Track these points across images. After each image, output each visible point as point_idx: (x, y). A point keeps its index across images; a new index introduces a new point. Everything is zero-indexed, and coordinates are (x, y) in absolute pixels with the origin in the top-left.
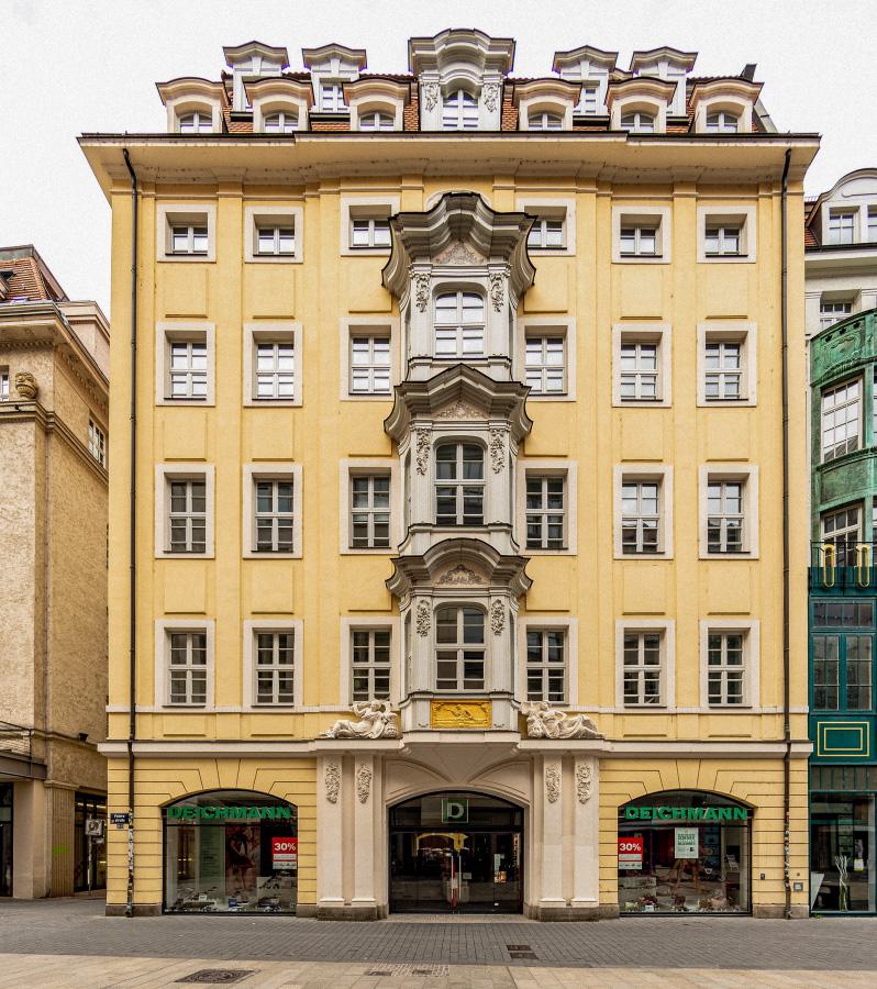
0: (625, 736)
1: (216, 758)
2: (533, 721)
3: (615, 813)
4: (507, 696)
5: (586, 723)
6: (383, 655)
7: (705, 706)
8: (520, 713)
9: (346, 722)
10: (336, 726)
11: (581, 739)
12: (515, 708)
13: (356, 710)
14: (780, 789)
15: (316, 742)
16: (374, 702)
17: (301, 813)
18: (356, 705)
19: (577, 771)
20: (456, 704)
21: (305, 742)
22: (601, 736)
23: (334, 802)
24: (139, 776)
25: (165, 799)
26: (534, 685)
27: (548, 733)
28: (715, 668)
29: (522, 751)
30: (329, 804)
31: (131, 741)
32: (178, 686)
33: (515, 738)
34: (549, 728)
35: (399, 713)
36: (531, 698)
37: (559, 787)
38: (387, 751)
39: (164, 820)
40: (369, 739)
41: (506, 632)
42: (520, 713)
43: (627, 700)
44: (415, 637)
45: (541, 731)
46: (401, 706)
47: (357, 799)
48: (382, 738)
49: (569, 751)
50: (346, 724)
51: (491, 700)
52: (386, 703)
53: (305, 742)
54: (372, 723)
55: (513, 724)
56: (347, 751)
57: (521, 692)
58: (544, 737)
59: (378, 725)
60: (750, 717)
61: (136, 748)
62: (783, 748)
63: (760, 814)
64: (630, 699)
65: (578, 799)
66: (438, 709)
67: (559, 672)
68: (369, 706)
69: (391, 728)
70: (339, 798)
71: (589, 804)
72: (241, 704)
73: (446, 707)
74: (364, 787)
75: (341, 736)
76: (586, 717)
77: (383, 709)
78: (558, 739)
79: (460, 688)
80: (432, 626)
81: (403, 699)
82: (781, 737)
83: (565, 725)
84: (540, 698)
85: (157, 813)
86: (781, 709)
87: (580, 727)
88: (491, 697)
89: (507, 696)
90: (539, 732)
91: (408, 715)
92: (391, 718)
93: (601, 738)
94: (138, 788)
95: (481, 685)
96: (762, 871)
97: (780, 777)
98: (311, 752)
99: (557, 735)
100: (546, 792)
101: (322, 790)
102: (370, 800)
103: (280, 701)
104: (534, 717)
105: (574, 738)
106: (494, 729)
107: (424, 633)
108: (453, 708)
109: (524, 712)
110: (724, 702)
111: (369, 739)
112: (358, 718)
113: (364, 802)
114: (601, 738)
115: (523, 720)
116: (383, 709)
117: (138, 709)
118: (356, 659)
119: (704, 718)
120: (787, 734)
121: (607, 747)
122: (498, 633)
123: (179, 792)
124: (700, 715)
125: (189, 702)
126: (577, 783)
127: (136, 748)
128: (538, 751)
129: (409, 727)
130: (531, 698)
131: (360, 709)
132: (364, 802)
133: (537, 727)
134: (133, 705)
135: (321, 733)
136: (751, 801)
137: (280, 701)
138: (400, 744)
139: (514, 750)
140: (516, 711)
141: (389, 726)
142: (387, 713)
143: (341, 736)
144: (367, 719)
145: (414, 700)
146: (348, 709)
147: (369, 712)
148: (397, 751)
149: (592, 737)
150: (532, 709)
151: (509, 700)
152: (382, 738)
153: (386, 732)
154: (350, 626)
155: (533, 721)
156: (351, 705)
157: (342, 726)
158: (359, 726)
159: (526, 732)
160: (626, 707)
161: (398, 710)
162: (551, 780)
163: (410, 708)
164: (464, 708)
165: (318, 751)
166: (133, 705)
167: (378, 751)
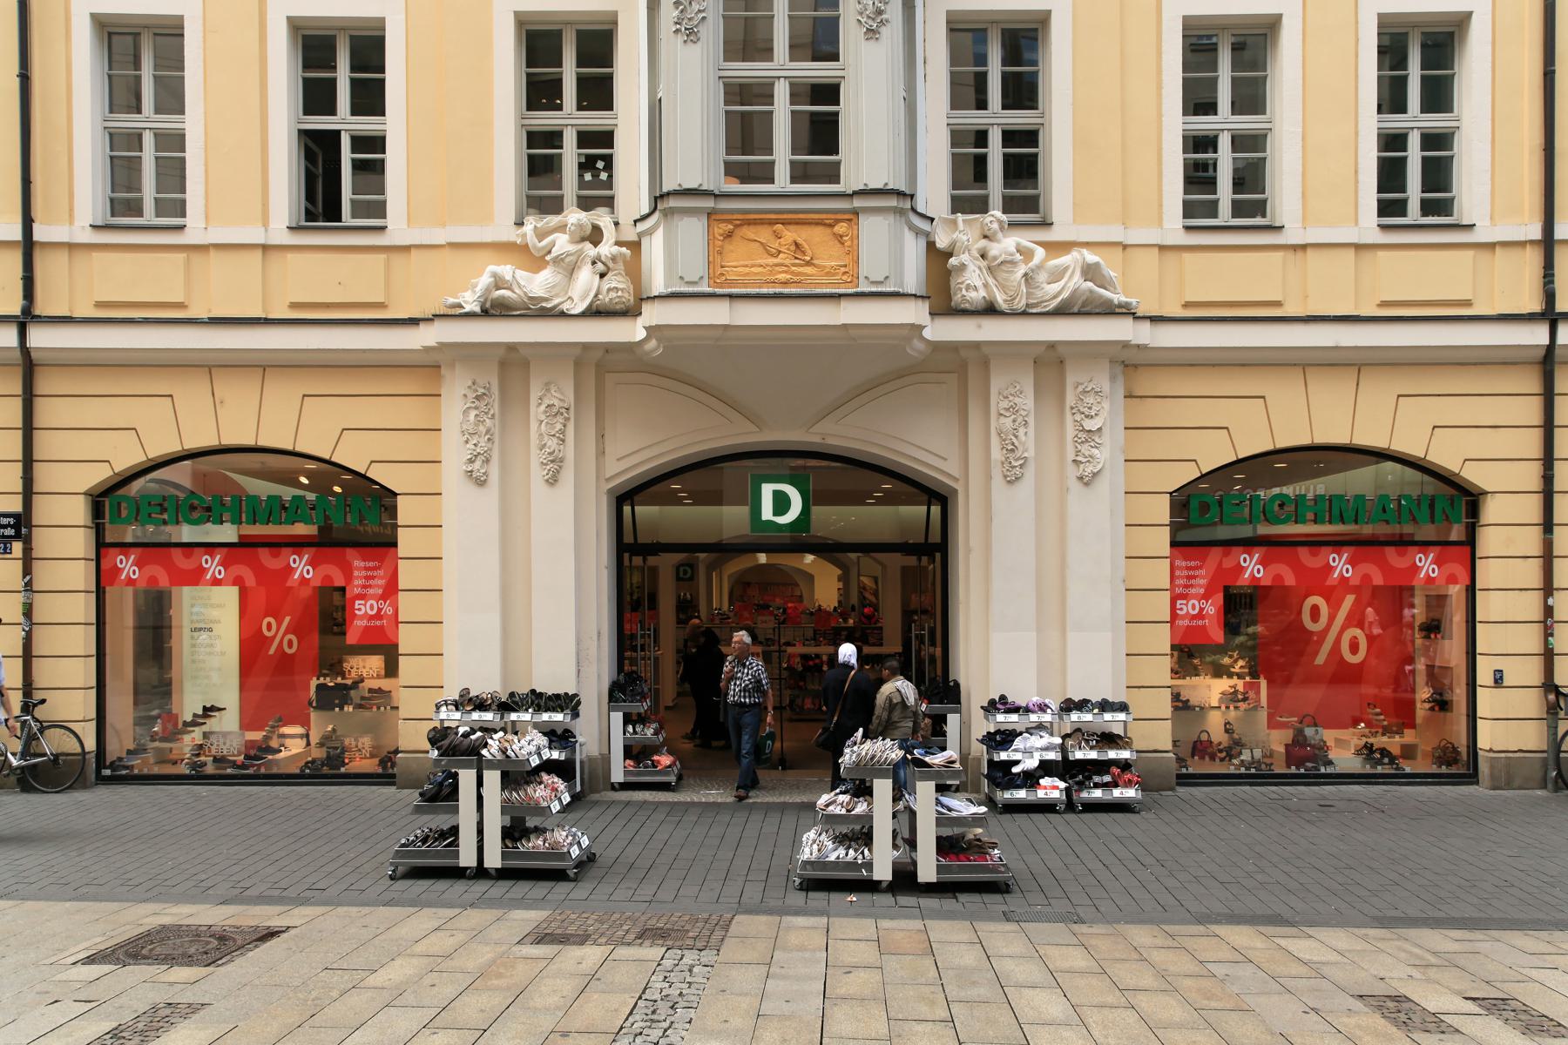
0: (1187, 305)
1: (210, 366)
2: (963, 267)
3: (1161, 510)
4: (900, 199)
5: (1090, 272)
6: (598, 93)
7: (1368, 224)
8: (931, 246)
9: (506, 271)
10: (485, 280)
11: (1080, 314)
12: (918, 232)
13: (531, 239)
14: (1531, 443)
15: (438, 324)
16: (574, 216)
17: (406, 510)
18: (532, 223)
19: (1070, 399)
20: (772, 223)
21: (413, 322)
22: (1127, 305)
23: (481, 482)
24: (46, 413)
25: (98, 476)
26: (971, 170)
27: (1000, 299)
28: (1203, 123)
29: (938, 347)
30: (471, 488)
31: (25, 320)
32: (123, 172)
33: (912, 313)
34: (1003, 287)
35: (635, 246)
36: (959, 205)
37: (1027, 441)
38: (609, 348)
39: (99, 530)
40: (563, 315)
41: (893, 32)
42: (931, 246)
43: (1189, 210)
44: (671, 43)
45: (982, 293)
46: (641, 227)
47: (538, 474)
48: (596, 312)
49: (1052, 346)
50: (508, 277)
51: (856, 212)
52: (602, 218)
53: (413, 322)
54: (571, 271)
55: (913, 274)
56: (512, 347)
57: (935, 190)
58: (990, 310)
59: (586, 278)
60: (1279, 255)
61: (40, 338)
62: (1537, 335)
63: (1492, 511)
64: (1197, 209)
65: (1072, 472)
66: (729, 236)
67: (1030, 137)
68: (562, 228)
69: (617, 287)
70: (494, 471)
71: (1102, 486)
72: (266, 224)
73: (749, 232)
74: (552, 444)
75: (493, 310)
76: (1091, 257)
77: (595, 236)
78: (1024, 314)
79: (782, 180)
80: (710, 15)
81: (646, 210)
82: (1535, 305)
83: (1042, 277)
84: (981, 206)
85: (79, 511)
86: (1535, 232)
87: (1074, 283)
88: (858, 203)
89: (900, 199)
90: (976, 296)
91: (655, 250)
92: (614, 259)
93: (1125, 311)
94: (45, 445)
95: (832, 174)
96: (1499, 663)
97: (1532, 411)
98: (427, 350)
99: (1020, 304)
100: (997, 454)
101: (454, 451)
102: (568, 476)
103: (794, 180)
104: (965, 258)
105: (1062, 311)
106: (864, 288)
107: (691, 35)
108: (764, 234)
109: (942, 242)
110: (1414, 212)
111: (563, 315)
112: (535, 260)
113: (553, 481)
114: (1125, 311)
115: (938, 258)
116: (595, 236)
117: (39, 234)
118: (533, 104)
119: (1171, 257)
120: (1550, 297)
121: (1143, 334)
122: (872, 33)
123: (127, 457)
124: (1162, 248)
125: (149, 216)
126: (1070, 431)
127: (40, 338)
128: (977, 345)
129: (658, 285)
130: (959, 205)
131: (541, 234)
132: (553, 481)
133: (973, 284)
134: (28, 222)
135: (451, 300)
136: (1474, 475)
137: (794, 180)
138: (632, 331)
139: (917, 344)
140: (922, 243)
141: (613, 281)
142: (606, 249)
143: (493, 310)
144: (558, 261)
145: (669, 213)
146: (509, 234)
147: (562, 244)
148: (629, 348)
149: (1110, 311)
150: (961, 234)
151: (900, 212)
152: (596, 312)
153: (605, 298)
154: (516, 14)
155: (963, 267)
156: (520, 224)
157: (499, 283)
158: (537, 284)
159: (948, 296)
160: (1188, 228)
161: (633, 237)
162: (1007, 423)
163: (658, 237)
164: (790, 234)
165: (443, 347)
166: (28, 222)
167: (586, 347)
